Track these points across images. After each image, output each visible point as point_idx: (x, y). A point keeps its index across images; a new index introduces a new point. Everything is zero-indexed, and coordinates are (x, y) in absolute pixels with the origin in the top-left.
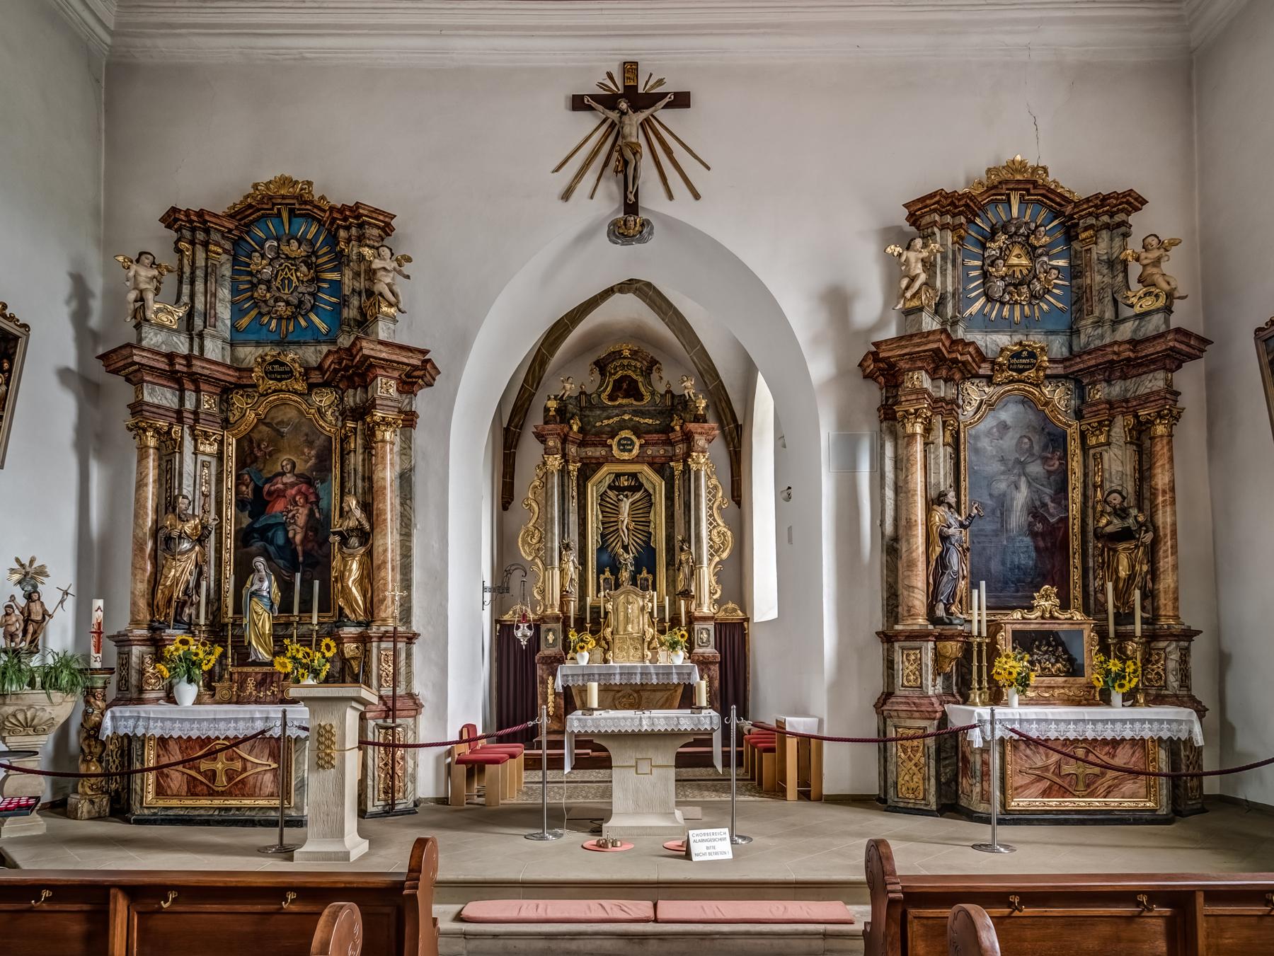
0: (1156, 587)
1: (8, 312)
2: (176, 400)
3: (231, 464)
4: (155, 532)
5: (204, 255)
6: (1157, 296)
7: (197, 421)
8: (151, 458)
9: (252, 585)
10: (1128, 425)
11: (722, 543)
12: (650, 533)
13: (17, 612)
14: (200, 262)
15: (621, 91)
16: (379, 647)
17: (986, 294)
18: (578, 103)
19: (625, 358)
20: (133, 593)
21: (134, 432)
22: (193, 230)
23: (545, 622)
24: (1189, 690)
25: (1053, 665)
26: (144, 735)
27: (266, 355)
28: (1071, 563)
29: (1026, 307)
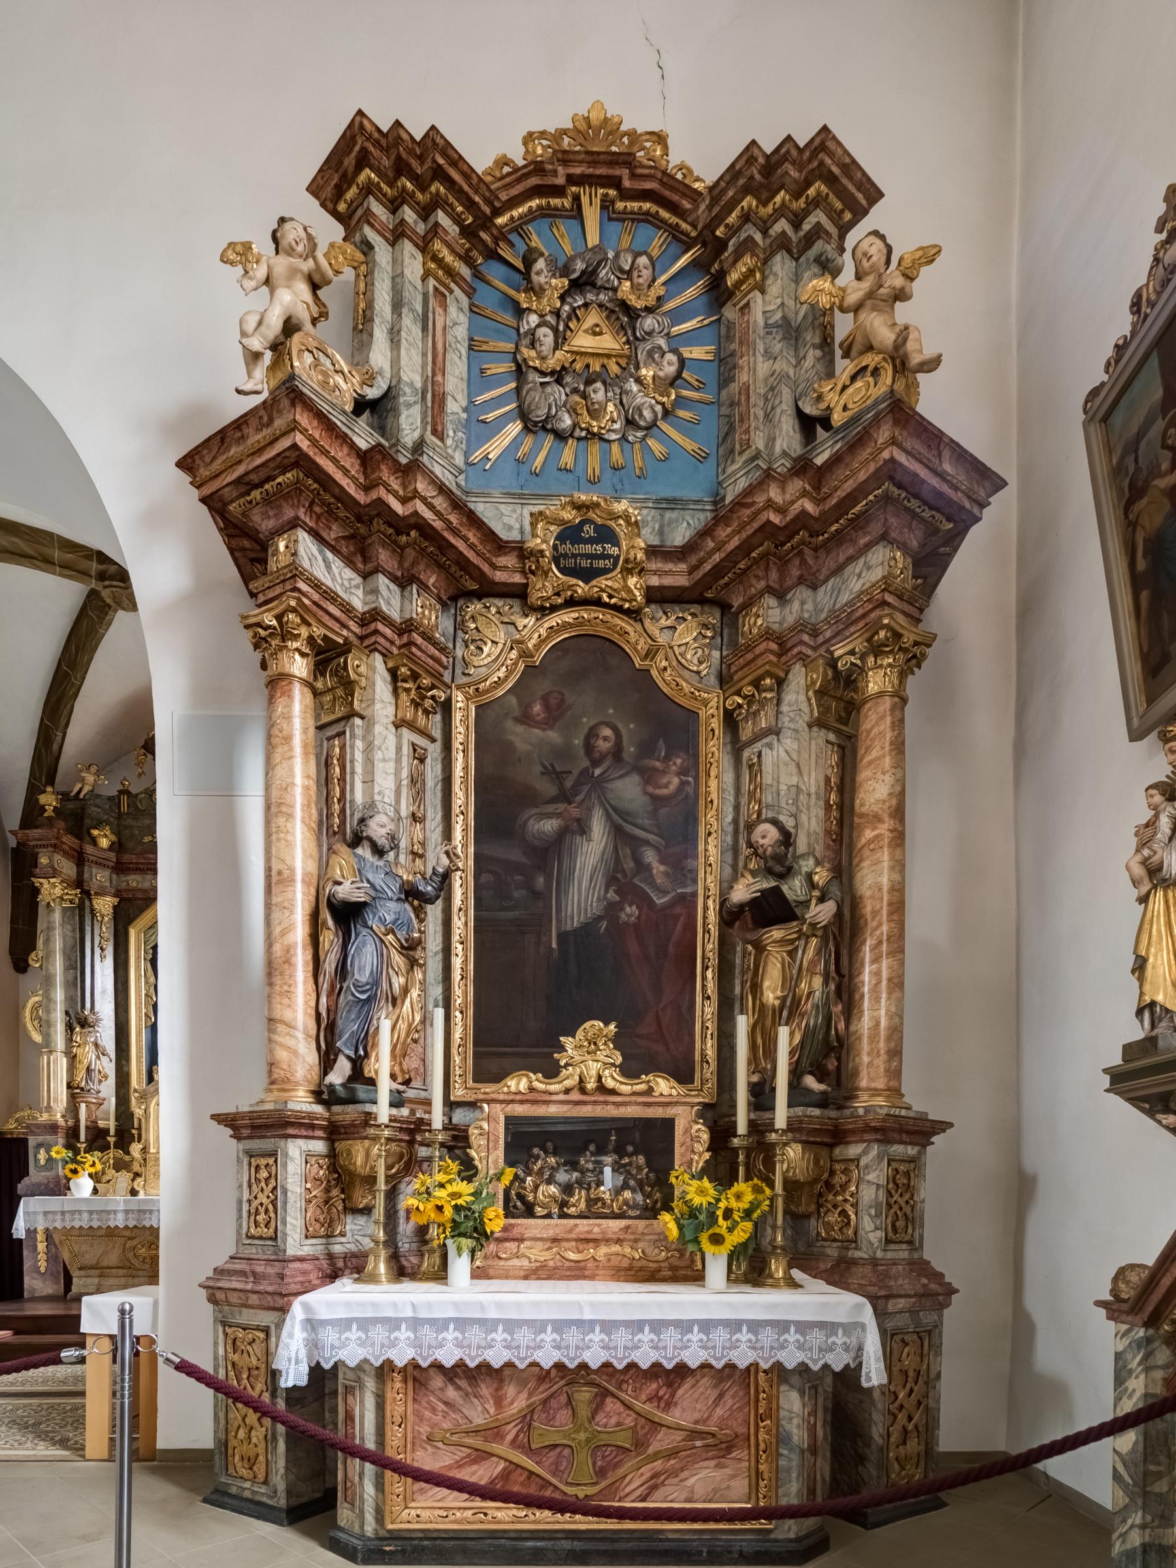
0: (852, 1028)
10: (813, 683)
17: (523, 414)
23: (33, 1133)
24: (914, 1245)
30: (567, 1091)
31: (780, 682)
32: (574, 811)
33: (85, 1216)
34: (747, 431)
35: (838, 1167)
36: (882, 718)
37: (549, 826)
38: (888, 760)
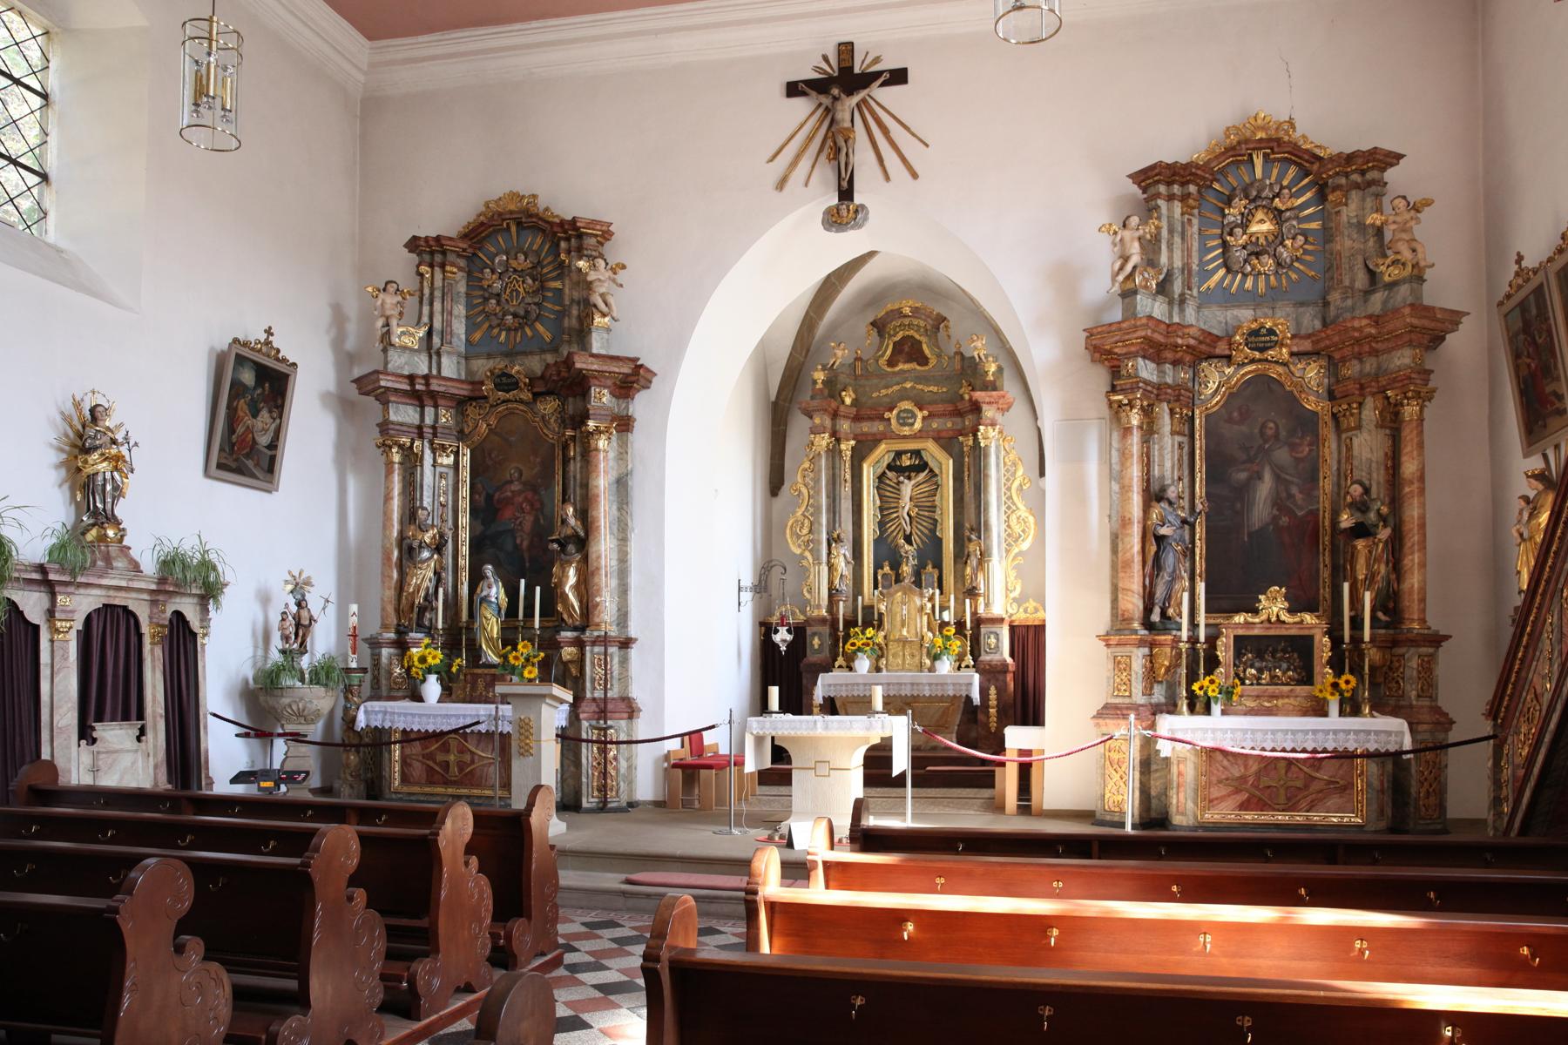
1: (280, 356)
2: (417, 416)
3: (466, 474)
4: (402, 538)
5: (441, 276)
6: (1404, 264)
7: (435, 435)
8: (396, 472)
9: (482, 591)
11: (1023, 531)
12: (936, 521)
13: (290, 618)
14: (438, 283)
15: (836, 74)
16: (592, 652)
18: (793, 90)
19: (906, 316)
20: (382, 599)
21: (382, 449)
22: (432, 253)
23: (810, 625)
25: (1284, 673)
26: (390, 728)
27: (495, 368)
28: (1321, 560)
29: (1272, 278)
30: (1262, 622)
31: (1360, 404)
32: (1256, 468)
33: (909, 687)
34: (1341, 275)
35: (1395, 659)
36: (1411, 432)
37: (1243, 476)
38: (1415, 453)
